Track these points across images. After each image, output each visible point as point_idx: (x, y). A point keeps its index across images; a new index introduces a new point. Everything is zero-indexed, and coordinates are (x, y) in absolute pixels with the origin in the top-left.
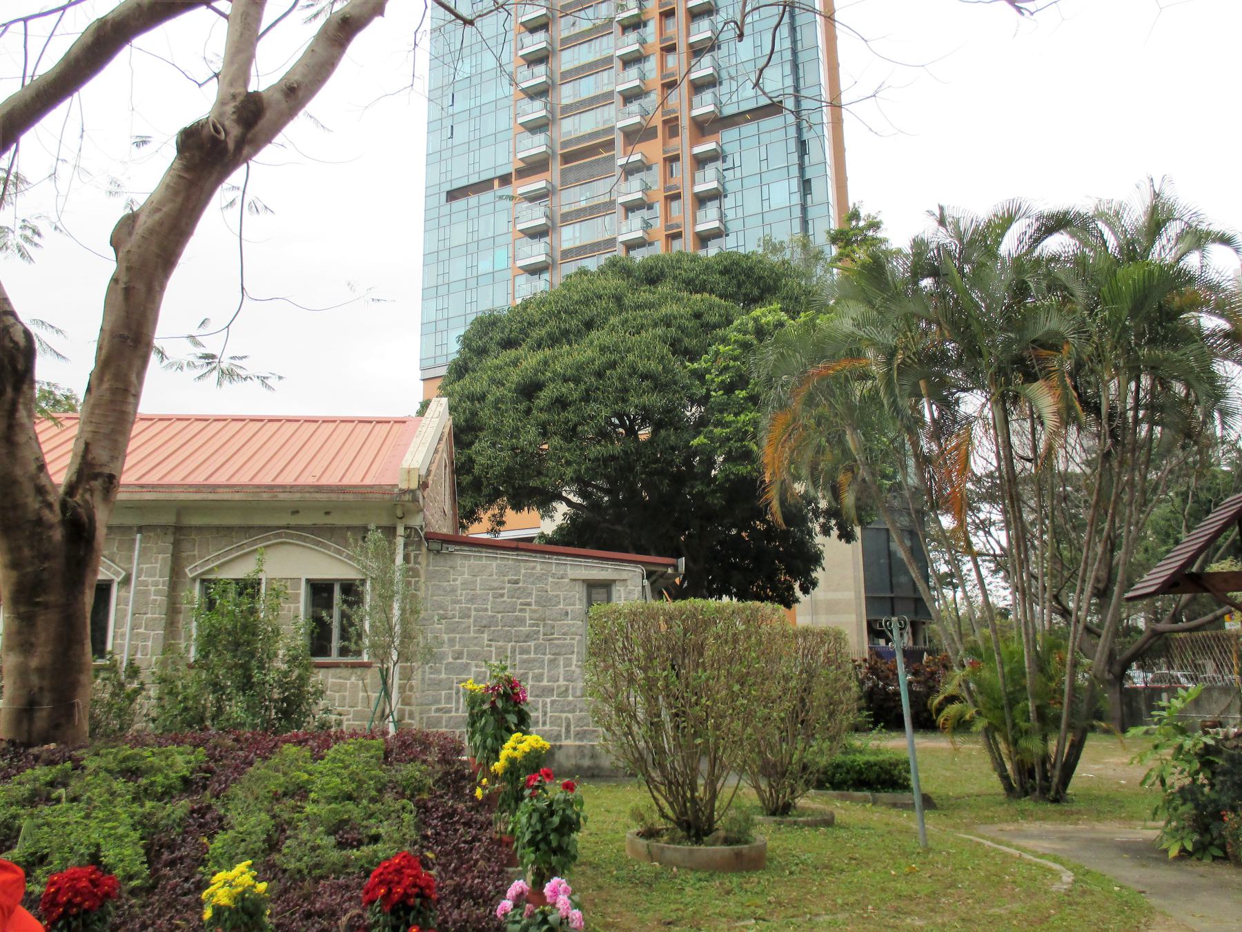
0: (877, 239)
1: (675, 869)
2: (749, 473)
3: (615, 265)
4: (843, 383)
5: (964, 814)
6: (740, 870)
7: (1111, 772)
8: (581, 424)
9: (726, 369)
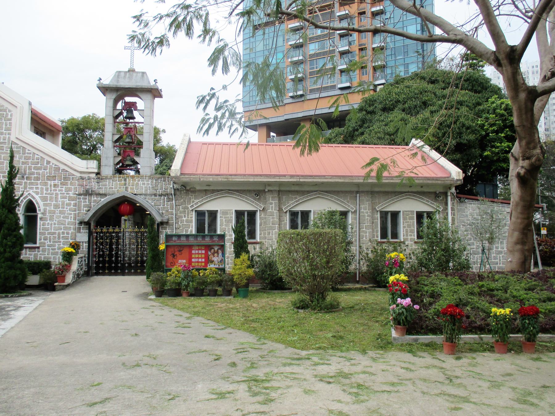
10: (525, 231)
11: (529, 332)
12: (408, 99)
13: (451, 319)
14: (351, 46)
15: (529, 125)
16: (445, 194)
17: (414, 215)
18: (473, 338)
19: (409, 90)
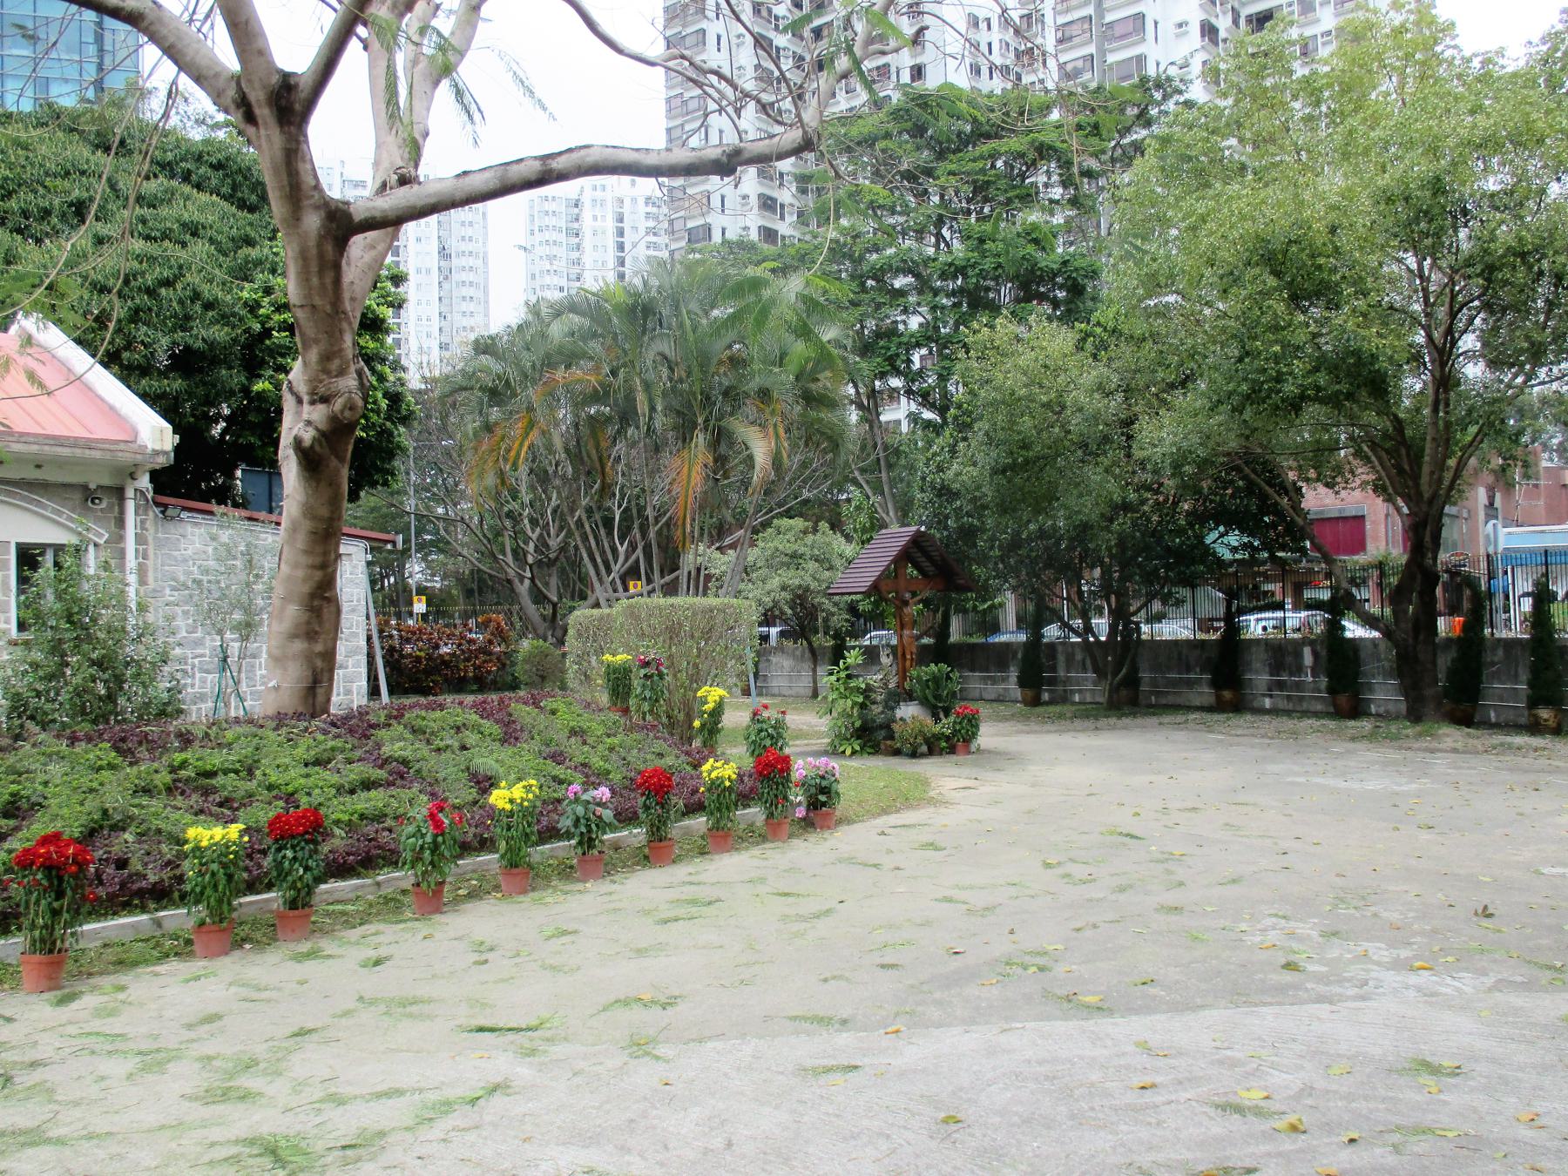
10: (316, 603)
11: (294, 882)
12: (20, 185)
13: (49, 877)
15: (328, 308)
16: (119, 493)
17: (8, 553)
18: (132, 925)
19: (27, 158)
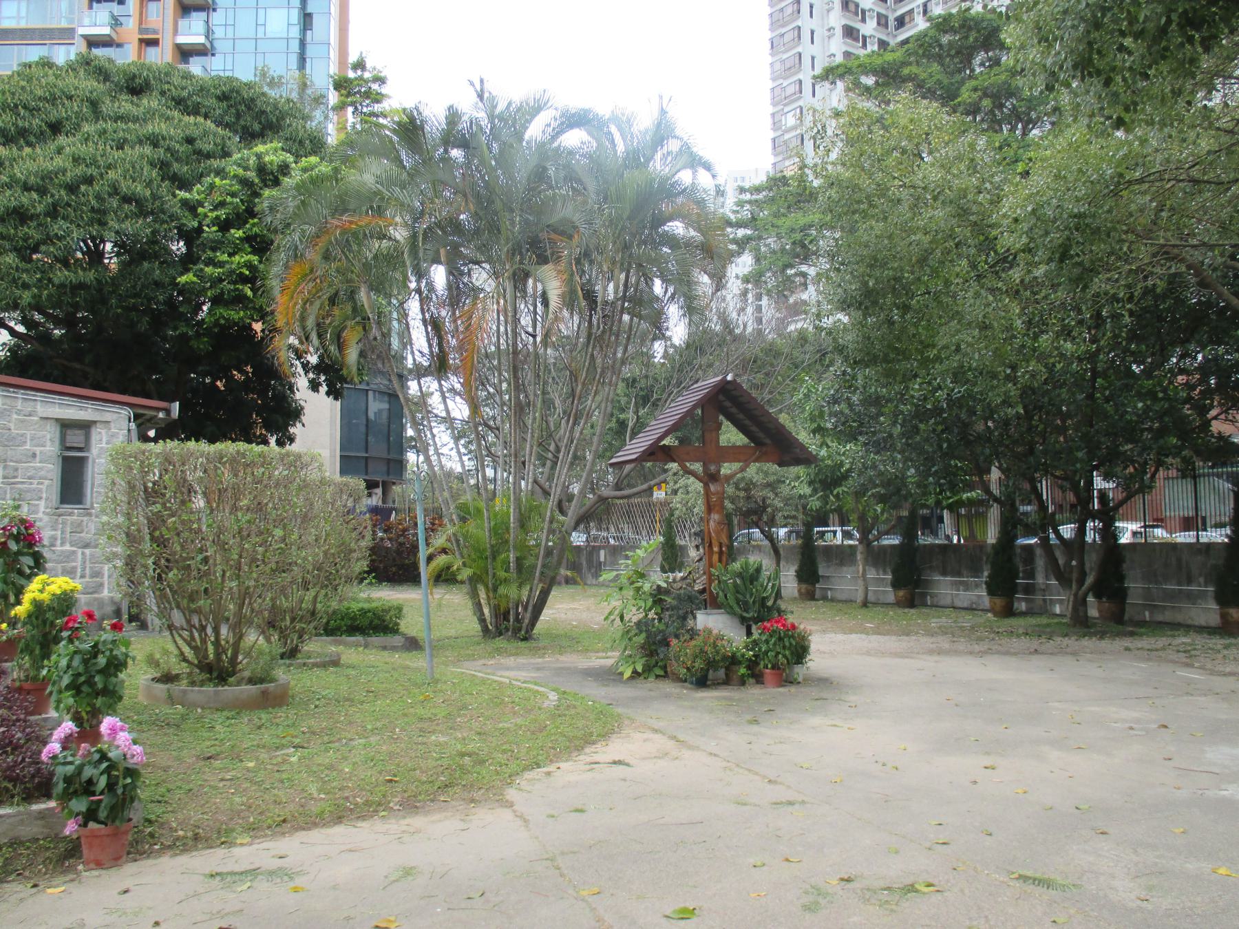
0: (380, 94)
1: (199, 710)
2: (242, 319)
3: (88, 64)
4: (360, 237)
5: (448, 653)
6: (265, 708)
7: (563, 616)
8: (44, 243)
9: (222, 204)
14: (118, 29)
